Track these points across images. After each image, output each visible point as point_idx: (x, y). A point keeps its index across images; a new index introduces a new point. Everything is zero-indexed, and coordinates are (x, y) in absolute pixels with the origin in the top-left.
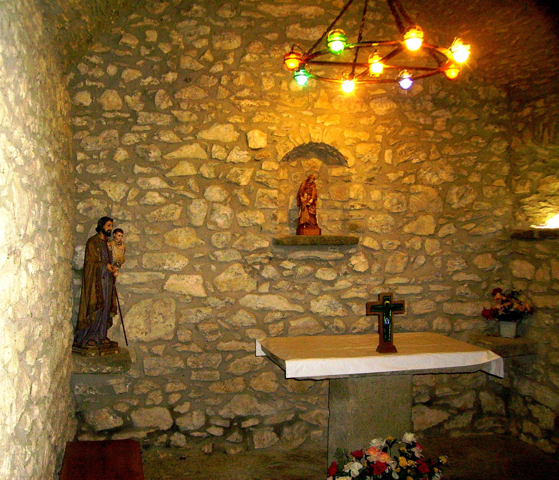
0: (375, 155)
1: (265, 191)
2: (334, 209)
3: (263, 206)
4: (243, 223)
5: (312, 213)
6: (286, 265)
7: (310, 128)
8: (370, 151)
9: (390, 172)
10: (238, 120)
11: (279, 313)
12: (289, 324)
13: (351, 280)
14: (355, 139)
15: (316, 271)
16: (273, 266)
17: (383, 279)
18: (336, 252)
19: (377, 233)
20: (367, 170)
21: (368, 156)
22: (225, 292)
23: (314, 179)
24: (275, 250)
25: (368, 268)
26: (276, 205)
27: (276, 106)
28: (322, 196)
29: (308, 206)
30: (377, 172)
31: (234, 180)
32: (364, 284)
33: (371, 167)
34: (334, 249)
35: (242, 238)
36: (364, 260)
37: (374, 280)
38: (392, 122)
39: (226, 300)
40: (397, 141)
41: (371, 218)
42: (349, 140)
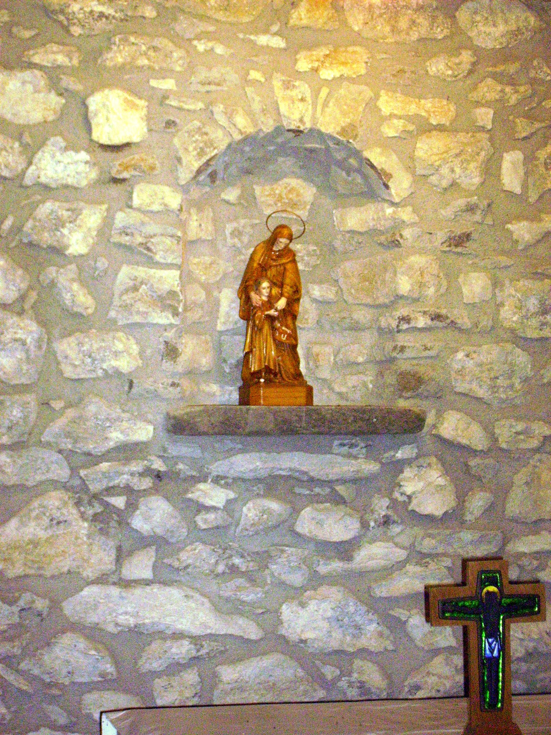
0: (472, 165)
1: (141, 272)
2: (351, 329)
3: (137, 319)
4: (75, 366)
5: (284, 338)
6: (206, 494)
7: (277, 84)
8: (457, 155)
9: (519, 218)
10: (61, 59)
11: (186, 642)
12: (215, 675)
13: (405, 540)
14: (409, 119)
15: (296, 511)
16: (167, 498)
17: (499, 537)
18: (356, 458)
19: (479, 399)
20: (447, 213)
21: (453, 171)
22: (18, 578)
23: (291, 238)
24: (174, 450)
25: (454, 504)
26: (176, 314)
27: (175, 19)
28: (316, 291)
29: (271, 319)
30: (478, 217)
31: (47, 239)
32: (444, 555)
33: (461, 202)
34: (352, 446)
35: (71, 413)
36: (441, 481)
37: (472, 542)
38: (526, 68)
39: (22, 603)
40: (537, 125)
41: (460, 355)
42: (395, 121)
